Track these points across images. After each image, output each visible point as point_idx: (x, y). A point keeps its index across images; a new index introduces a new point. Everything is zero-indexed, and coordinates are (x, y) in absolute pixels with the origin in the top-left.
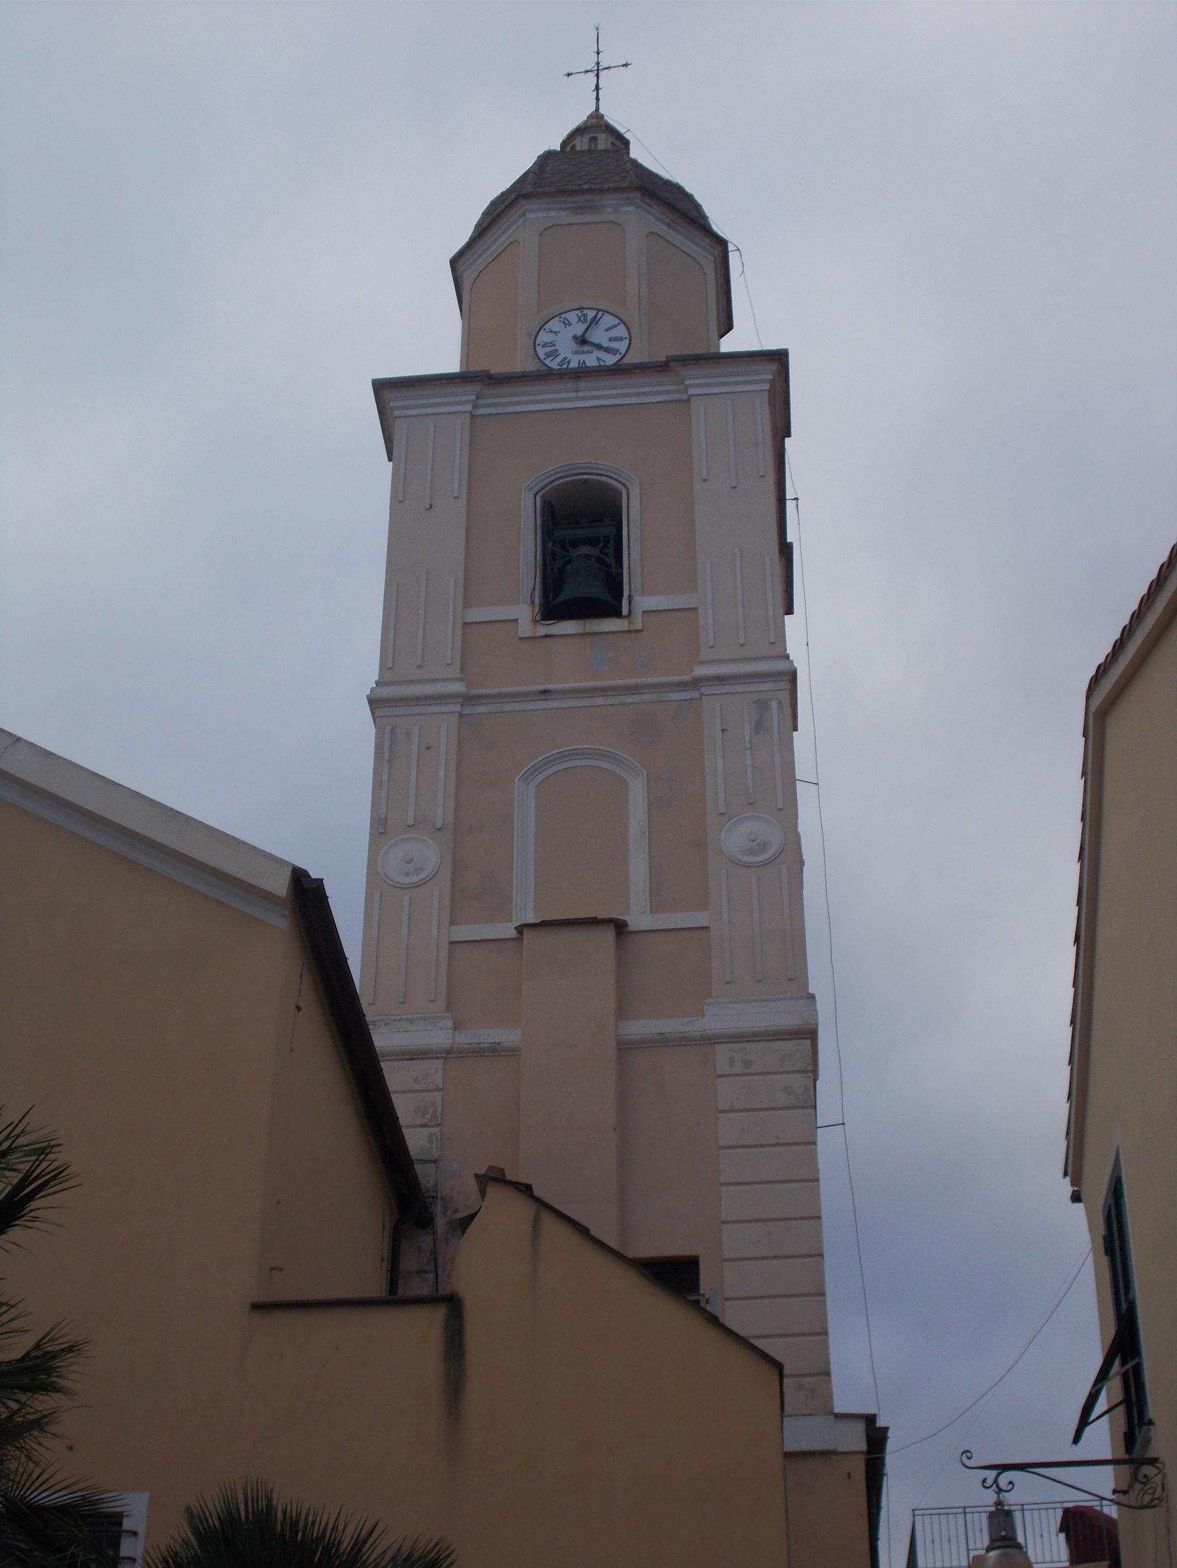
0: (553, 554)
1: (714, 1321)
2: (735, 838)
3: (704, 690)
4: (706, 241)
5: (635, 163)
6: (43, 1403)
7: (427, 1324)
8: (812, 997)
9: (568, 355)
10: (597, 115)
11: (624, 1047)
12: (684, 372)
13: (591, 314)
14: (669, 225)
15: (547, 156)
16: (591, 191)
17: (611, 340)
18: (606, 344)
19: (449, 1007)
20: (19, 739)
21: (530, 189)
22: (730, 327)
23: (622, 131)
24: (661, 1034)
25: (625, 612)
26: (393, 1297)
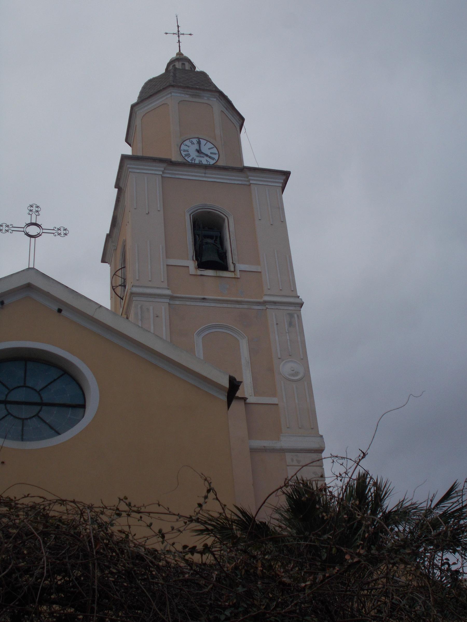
2: (286, 368)
8: (322, 436)
10: (180, 54)
11: (253, 451)
12: (249, 173)
14: (226, 109)
16: (199, 89)
17: (211, 153)
18: (209, 155)
20: (101, 306)
24: (264, 447)
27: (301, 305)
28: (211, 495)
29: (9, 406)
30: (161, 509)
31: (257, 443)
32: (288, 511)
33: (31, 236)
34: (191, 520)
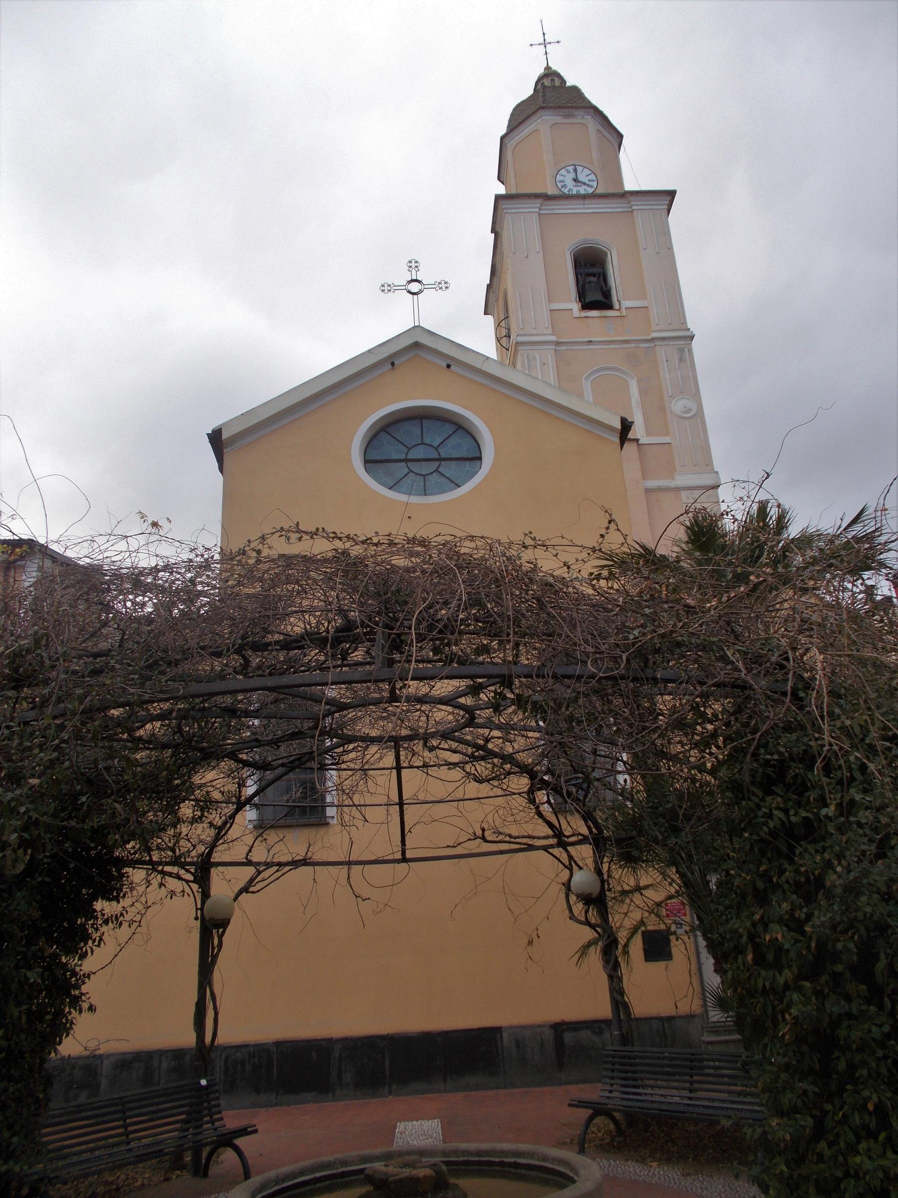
2: (678, 406)
3: (657, 343)
9: (571, 187)
10: (548, 68)
11: (648, 491)
12: (631, 198)
18: (587, 182)
27: (692, 338)
28: (612, 526)
29: (409, 464)
30: (565, 542)
31: (652, 484)
32: (687, 543)
33: (413, 294)
34: (594, 550)
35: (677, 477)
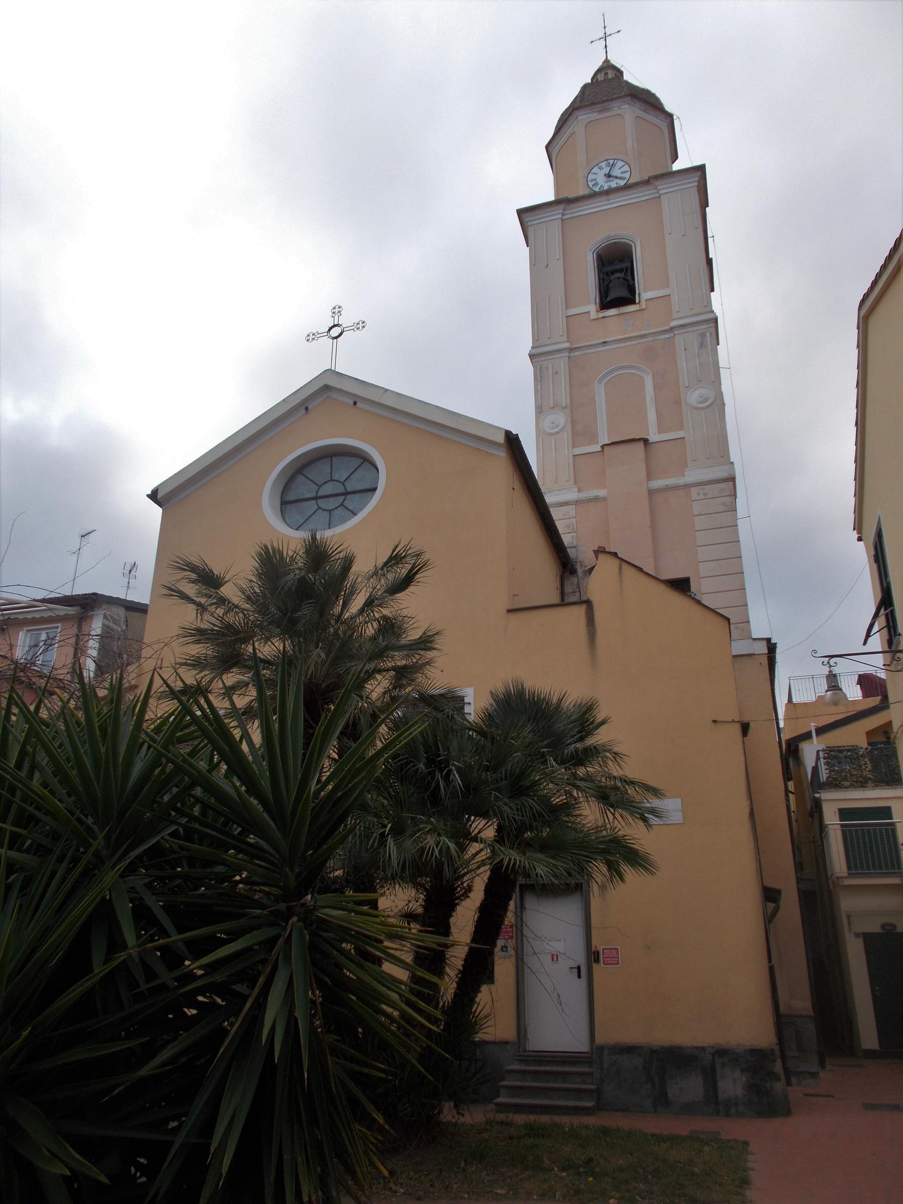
0: (603, 279)
1: (699, 602)
2: (693, 397)
4: (662, 116)
5: (627, 82)
6: (430, 654)
7: (579, 612)
9: (603, 184)
10: (607, 61)
11: (651, 493)
12: (656, 183)
13: (611, 162)
15: (585, 87)
16: (607, 101)
18: (619, 175)
19: (575, 483)
21: (578, 104)
22: (676, 158)
23: (619, 66)
25: (637, 301)
26: (563, 602)
35: (686, 473)
